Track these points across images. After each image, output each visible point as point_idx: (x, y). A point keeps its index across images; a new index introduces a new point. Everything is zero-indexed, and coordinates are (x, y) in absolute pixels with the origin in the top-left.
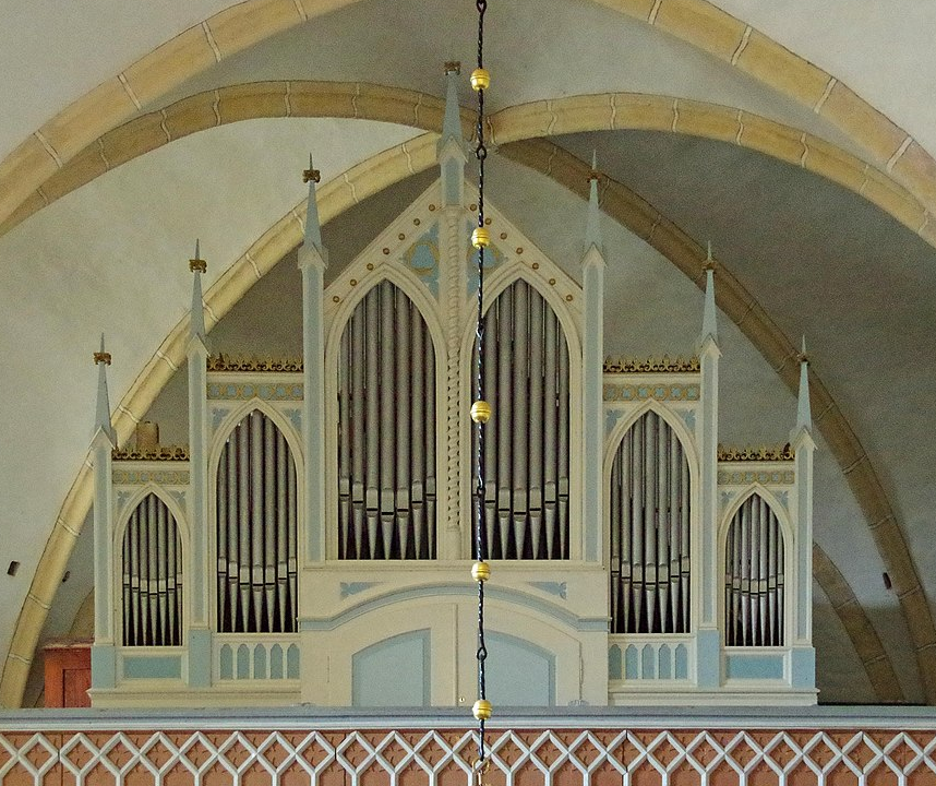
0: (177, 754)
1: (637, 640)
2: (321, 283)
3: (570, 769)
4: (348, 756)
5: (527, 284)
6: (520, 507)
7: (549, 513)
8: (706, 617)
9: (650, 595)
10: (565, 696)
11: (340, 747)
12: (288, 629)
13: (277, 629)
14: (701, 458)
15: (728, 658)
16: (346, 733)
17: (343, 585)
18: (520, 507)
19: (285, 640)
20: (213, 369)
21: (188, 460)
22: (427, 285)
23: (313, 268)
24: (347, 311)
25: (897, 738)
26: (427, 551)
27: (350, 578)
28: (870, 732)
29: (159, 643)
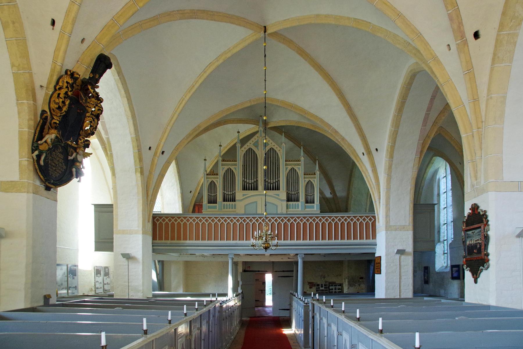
1: (291, 203)
6: (272, 182)
9: (293, 196)
12: (234, 201)
13: (232, 201)
15: (306, 206)
18: (272, 182)
19: (233, 203)
26: (256, 189)
28: (328, 217)
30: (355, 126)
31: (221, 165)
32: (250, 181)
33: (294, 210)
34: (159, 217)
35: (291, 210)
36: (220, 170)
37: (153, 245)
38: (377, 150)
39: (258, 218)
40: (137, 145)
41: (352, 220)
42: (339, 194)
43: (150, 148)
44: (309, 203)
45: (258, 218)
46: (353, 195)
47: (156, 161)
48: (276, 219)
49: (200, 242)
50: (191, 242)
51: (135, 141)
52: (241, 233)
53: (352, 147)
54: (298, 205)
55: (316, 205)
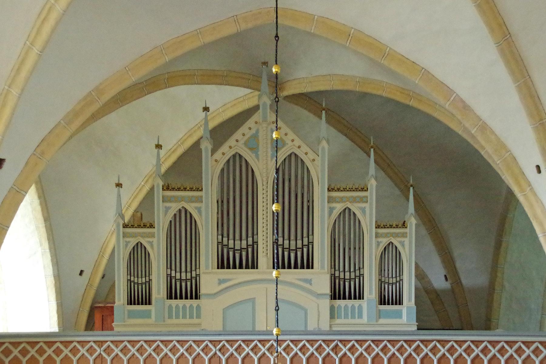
0: (150, 350)
2: (210, 154)
6: (293, 247)
7: (305, 250)
8: (370, 293)
9: (347, 284)
11: (218, 347)
12: (196, 298)
13: (191, 298)
15: (380, 310)
16: (220, 341)
17: (219, 280)
19: (194, 302)
20: (165, 190)
21: (154, 228)
23: (206, 148)
25: (450, 344)
28: (439, 341)
29: (142, 304)
30: (519, 89)
32: (238, 243)
41: (502, 351)
44: (389, 304)
46: (507, 284)
53: (508, 151)
55: (408, 308)
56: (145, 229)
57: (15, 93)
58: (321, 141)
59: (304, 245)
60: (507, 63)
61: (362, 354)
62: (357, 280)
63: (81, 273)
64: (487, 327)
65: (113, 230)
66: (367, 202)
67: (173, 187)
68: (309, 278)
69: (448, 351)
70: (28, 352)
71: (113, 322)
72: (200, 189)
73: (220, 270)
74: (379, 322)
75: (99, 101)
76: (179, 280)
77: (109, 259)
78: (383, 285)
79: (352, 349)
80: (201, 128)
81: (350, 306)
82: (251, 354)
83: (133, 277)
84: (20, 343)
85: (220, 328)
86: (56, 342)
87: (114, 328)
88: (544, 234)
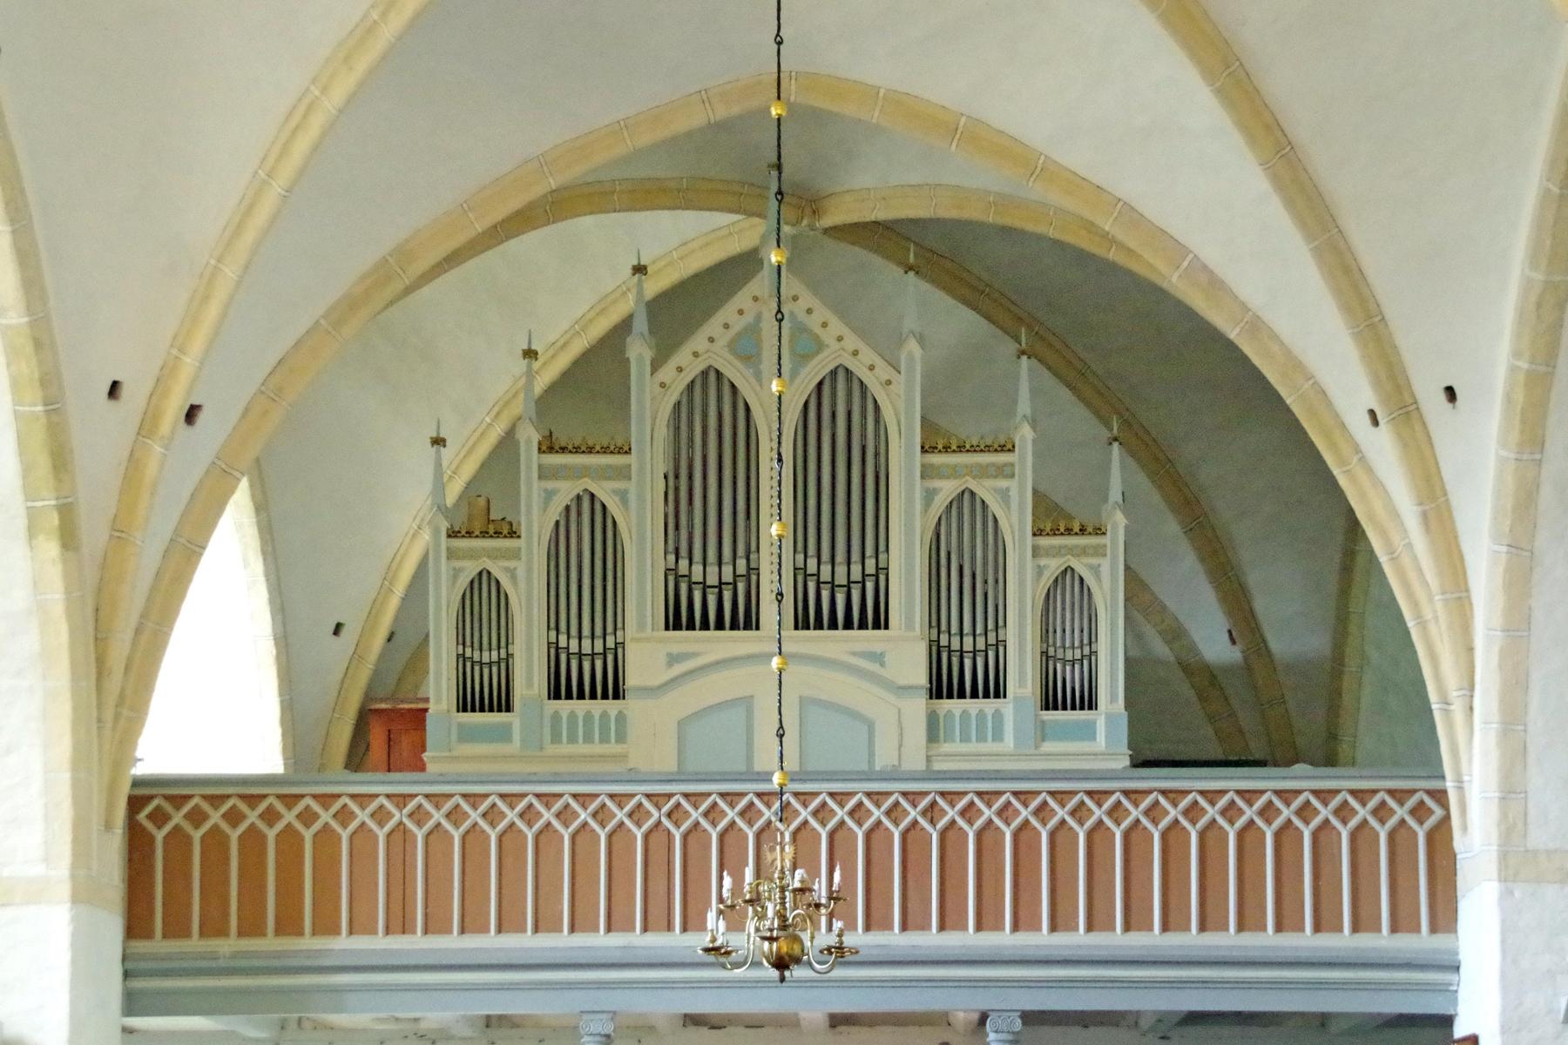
0: (511, 815)
1: (952, 707)
2: (648, 369)
3: (882, 828)
4: (633, 817)
5: (847, 370)
6: (841, 579)
7: (870, 585)
8: (1021, 682)
9: (968, 663)
10: (885, 757)
11: (665, 809)
12: (616, 696)
13: (605, 696)
14: (1017, 534)
15: (1043, 722)
16: (670, 796)
17: (669, 655)
18: (841, 579)
19: (612, 706)
20: (544, 452)
21: (519, 537)
22: (751, 371)
23: (640, 358)
24: (673, 397)
25: (1190, 797)
26: (750, 621)
27: (675, 649)
28: (1164, 792)
29: (491, 710)
30: (1318, 253)
31: (535, 474)
32: (712, 570)
33: (972, 747)
34: (166, 797)
35: (957, 747)
36: (529, 507)
37: (130, 965)
38: (1450, 393)
39: (901, 800)
40: (36, 376)
41: (1305, 812)
42: (1279, 645)
43: (114, 389)
44: (1065, 708)
45: (901, 800)
46: (1373, 654)
47: (152, 469)
48: (860, 804)
49: (417, 943)
50: (361, 943)
51: (29, 349)
52: (658, 886)
53: (1309, 377)
54: (998, 716)
55: (1110, 718)
56: (499, 540)
57: (230, 274)
58: (905, 340)
59: (867, 575)
60: (1290, 204)
61: (990, 821)
62: (991, 654)
63: (338, 629)
64: (1330, 760)
65: (416, 527)
66: (1013, 476)
67: (563, 444)
68: (879, 651)
69: (1186, 813)
70: (279, 816)
71: (424, 751)
72: (626, 448)
73: (672, 633)
74: (1042, 749)
75: (403, 276)
76: (577, 656)
77: (406, 595)
78: (1051, 663)
79: (969, 812)
80: (630, 295)
81: (974, 713)
82: (740, 823)
83: (470, 649)
84: (225, 797)
85: (671, 765)
86: (303, 796)
87: (427, 765)
88: (1390, 556)
